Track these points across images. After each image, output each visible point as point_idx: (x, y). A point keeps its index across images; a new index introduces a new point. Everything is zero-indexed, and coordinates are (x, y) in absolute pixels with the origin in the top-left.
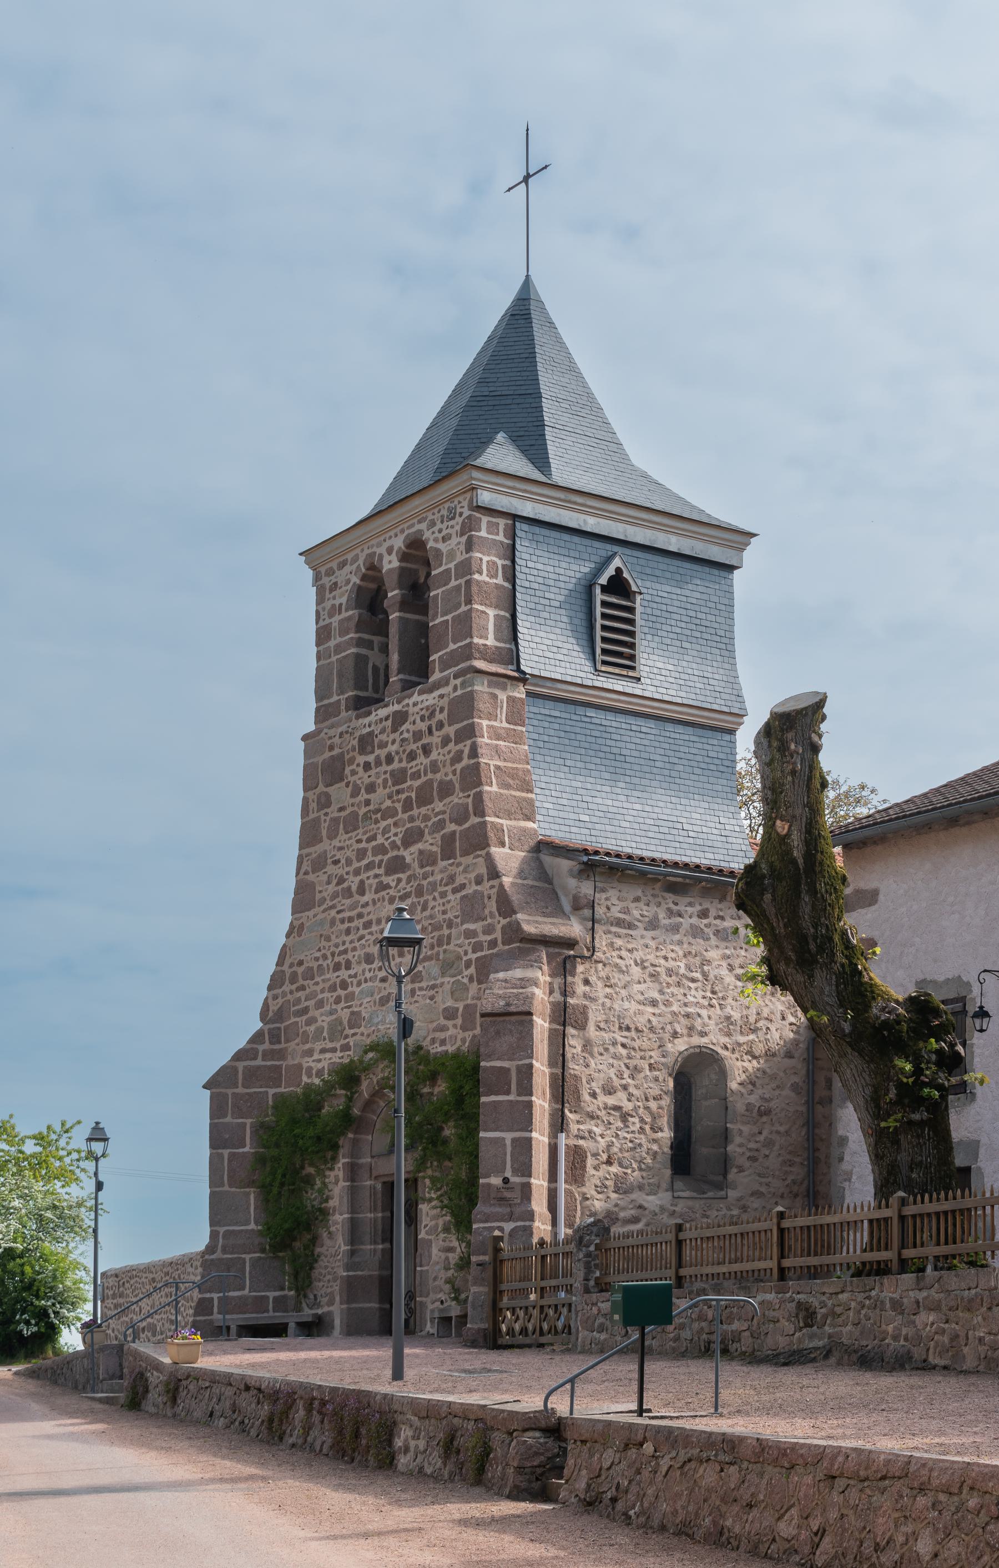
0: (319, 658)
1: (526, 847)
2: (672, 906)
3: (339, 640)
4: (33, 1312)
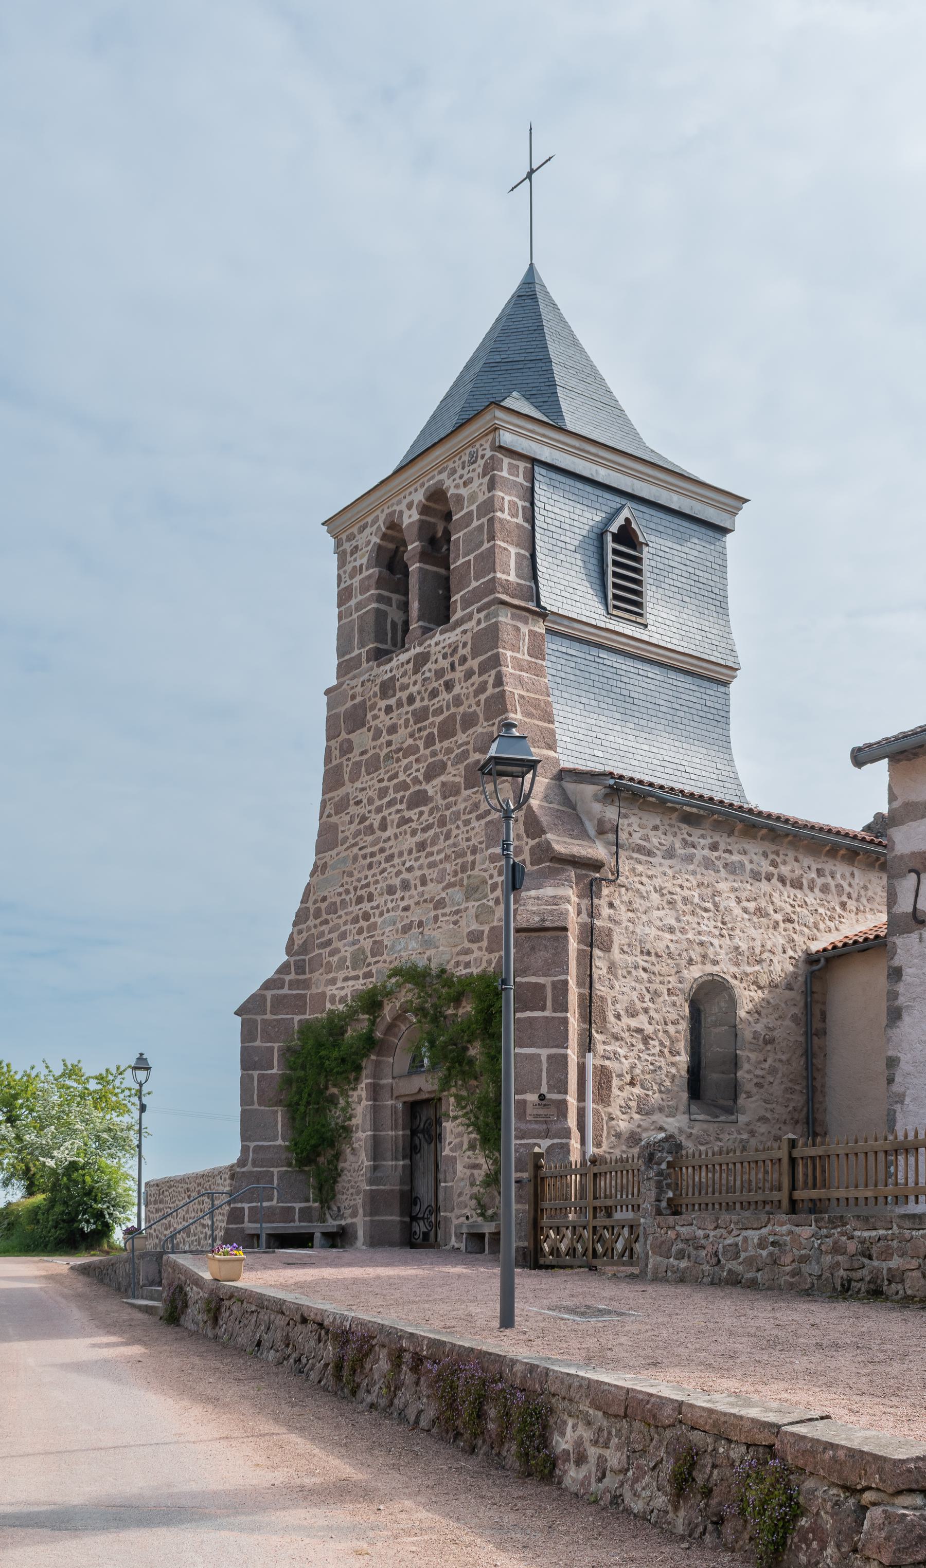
1: (549, 775)
2: (686, 836)
3: (360, 598)
4: (92, 1213)
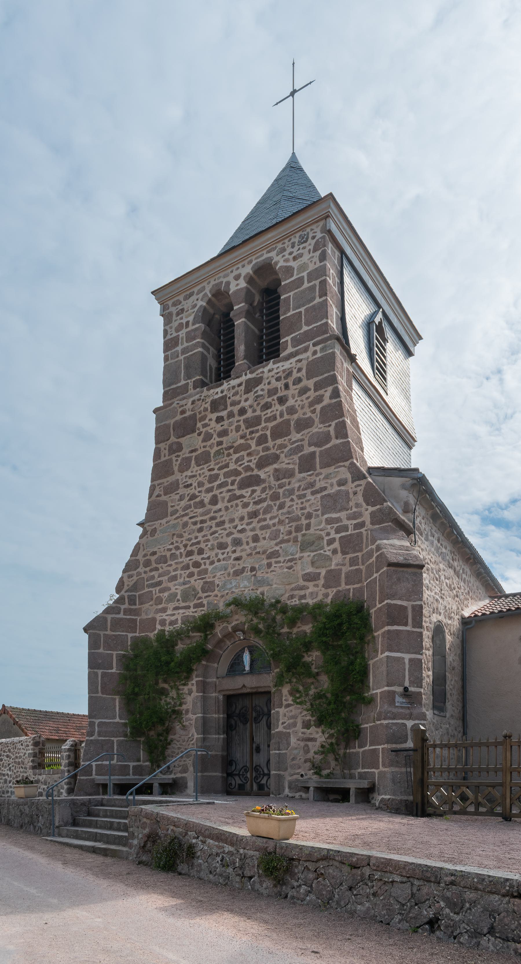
0: (166, 359)
3: (186, 345)
